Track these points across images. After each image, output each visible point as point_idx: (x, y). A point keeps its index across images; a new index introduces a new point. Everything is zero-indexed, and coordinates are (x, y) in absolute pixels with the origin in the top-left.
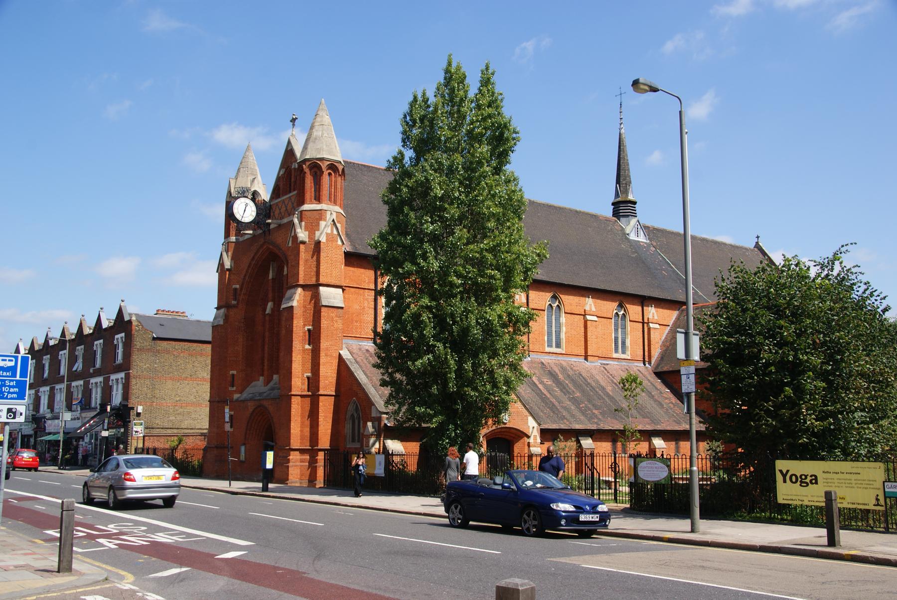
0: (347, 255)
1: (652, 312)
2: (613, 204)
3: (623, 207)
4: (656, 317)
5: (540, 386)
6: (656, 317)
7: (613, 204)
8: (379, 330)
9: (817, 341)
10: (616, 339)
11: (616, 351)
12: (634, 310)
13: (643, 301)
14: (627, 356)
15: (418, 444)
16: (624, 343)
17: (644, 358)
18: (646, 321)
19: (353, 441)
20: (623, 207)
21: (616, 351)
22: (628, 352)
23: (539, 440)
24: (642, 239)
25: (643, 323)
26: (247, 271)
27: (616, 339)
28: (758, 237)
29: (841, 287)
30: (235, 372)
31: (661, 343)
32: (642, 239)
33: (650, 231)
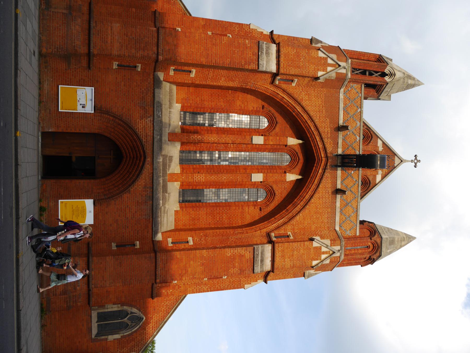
19: (101, 317)
26: (306, 112)
30: (193, 75)
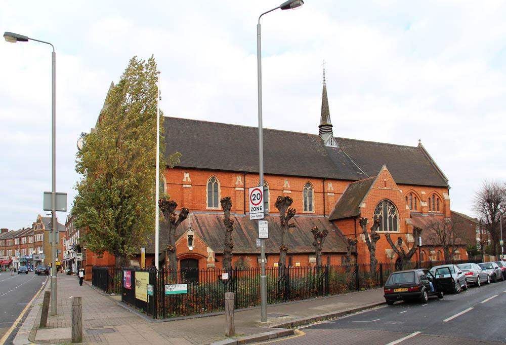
0: (291, 201)
1: (330, 186)
2: (319, 127)
3: (326, 127)
4: (332, 189)
5: (244, 230)
6: (332, 189)
7: (319, 127)
8: (346, 237)
9: (131, 97)
10: (305, 203)
11: (306, 209)
12: (317, 185)
13: (324, 179)
14: (313, 211)
15: (136, 272)
16: (311, 205)
17: (324, 212)
18: (325, 191)
20: (326, 127)
21: (306, 209)
22: (313, 210)
23: (213, 260)
24: (335, 145)
25: (324, 193)
27: (305, 203)
28: (420, 141)
29: (420, 150)
31: (336, 204)
32: (335, 145)
33: (338, 140)
